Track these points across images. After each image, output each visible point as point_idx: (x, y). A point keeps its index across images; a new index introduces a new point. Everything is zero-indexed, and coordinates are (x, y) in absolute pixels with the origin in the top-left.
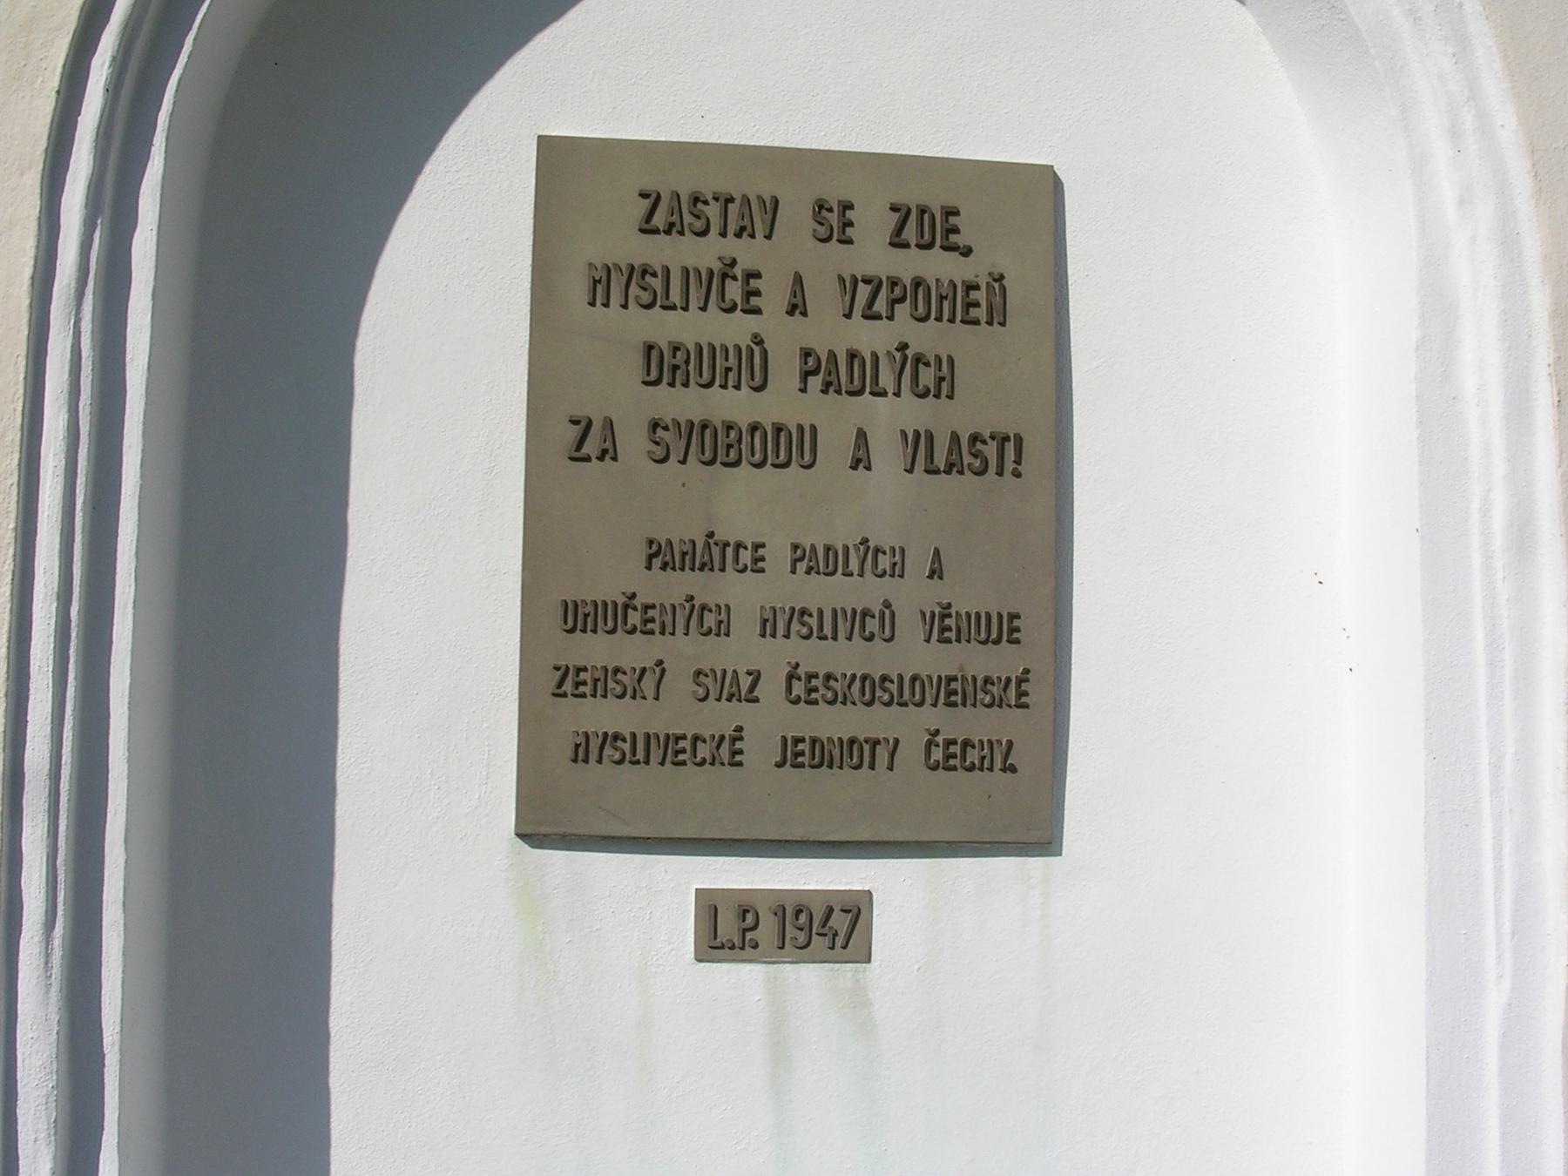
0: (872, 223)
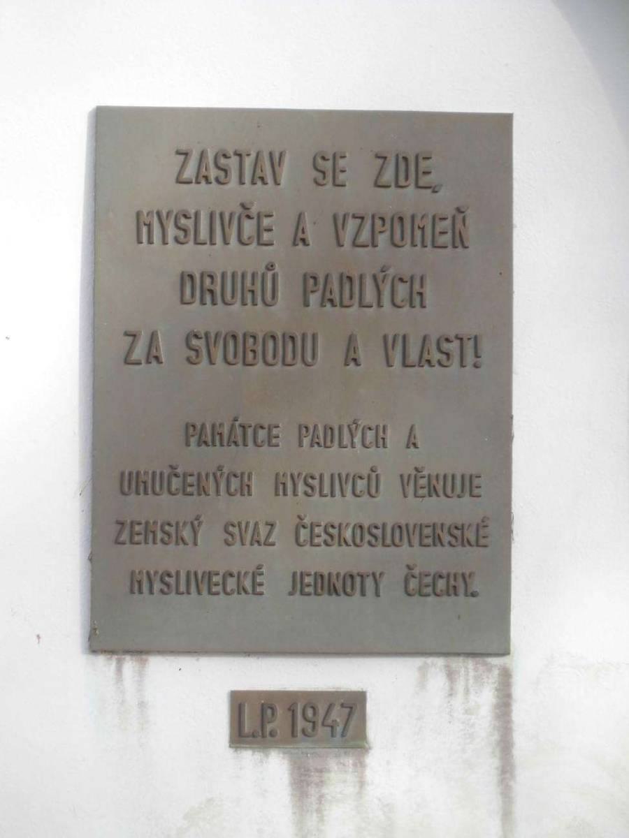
0: (358, 171)
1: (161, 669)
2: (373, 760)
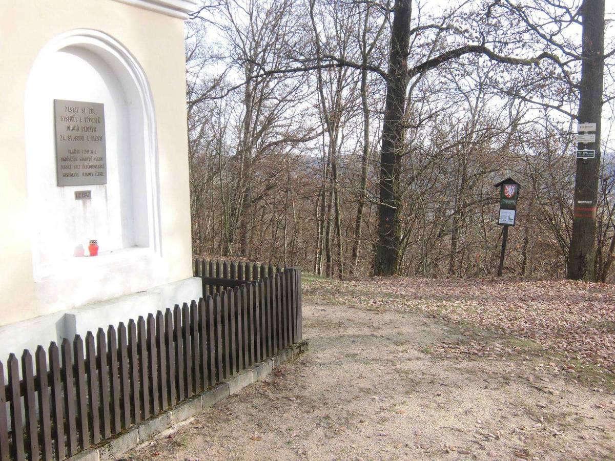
0: (87, 111)
1: (66, 188)
2: (92, 200)
